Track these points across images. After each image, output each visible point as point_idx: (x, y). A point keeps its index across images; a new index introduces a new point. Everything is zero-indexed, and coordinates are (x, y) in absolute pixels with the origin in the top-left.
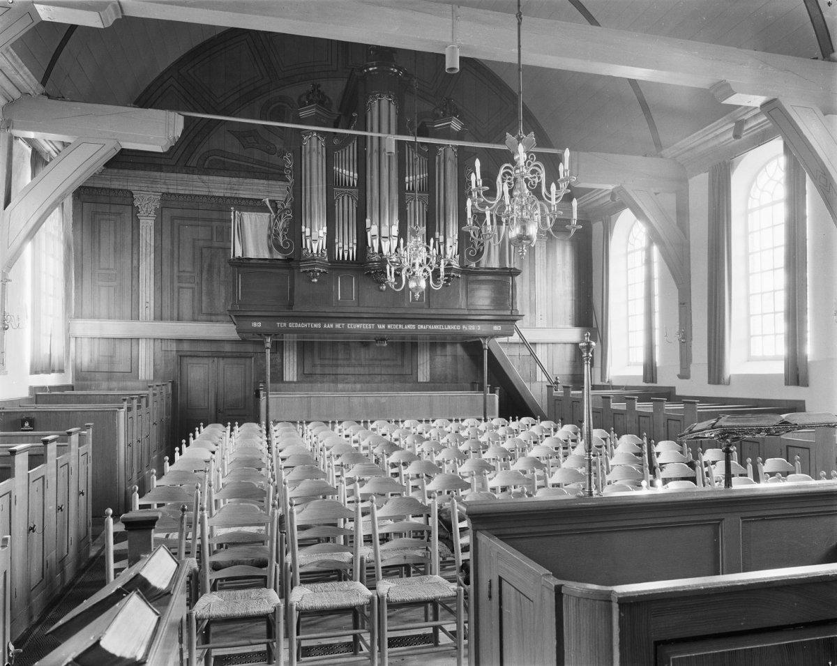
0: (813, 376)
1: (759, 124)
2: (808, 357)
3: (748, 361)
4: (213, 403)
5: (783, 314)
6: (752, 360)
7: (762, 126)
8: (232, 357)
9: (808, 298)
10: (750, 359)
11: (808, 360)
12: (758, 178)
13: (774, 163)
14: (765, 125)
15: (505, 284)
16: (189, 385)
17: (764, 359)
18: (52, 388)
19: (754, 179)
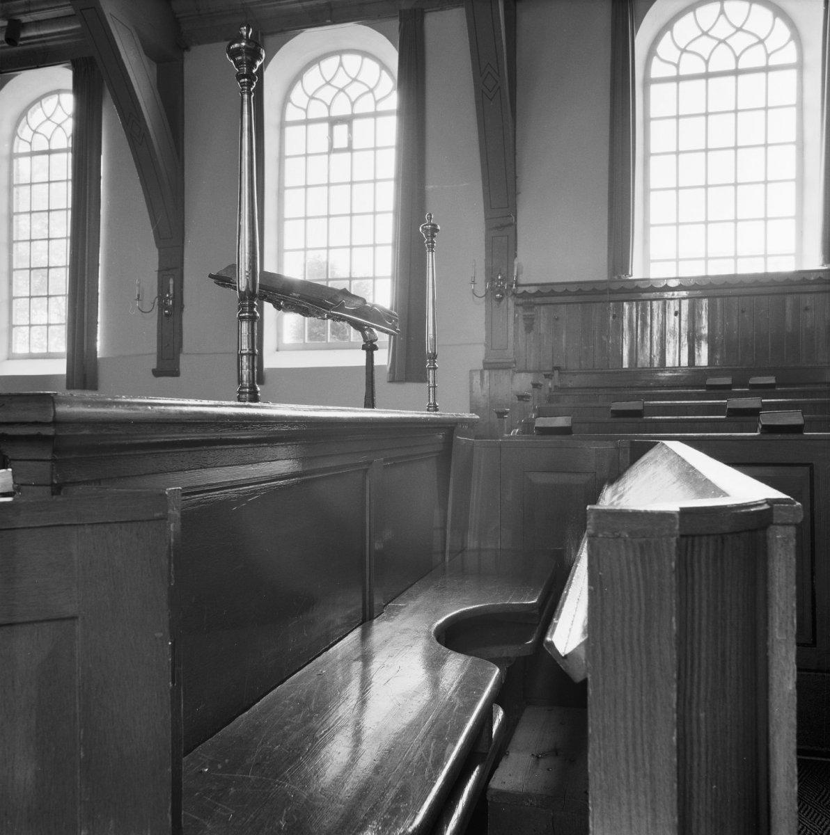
0: (104, 375)
1: (41, 36)
2: (98, 353)
3: (8, 359)
4: (14, 620)
5: (732, 272)
6: (13, 359)
7: (44, 41)
8: (802, 74)
9: (99, 286)
10: (11, 357)
11: (98, 357)
12: (29, 113)
13: (50, 104)
14: (49, 41)
15: (334, 149)
16: (171, 476)
17: (31, 357)
18: (623, 326)
19: (24, 113)
